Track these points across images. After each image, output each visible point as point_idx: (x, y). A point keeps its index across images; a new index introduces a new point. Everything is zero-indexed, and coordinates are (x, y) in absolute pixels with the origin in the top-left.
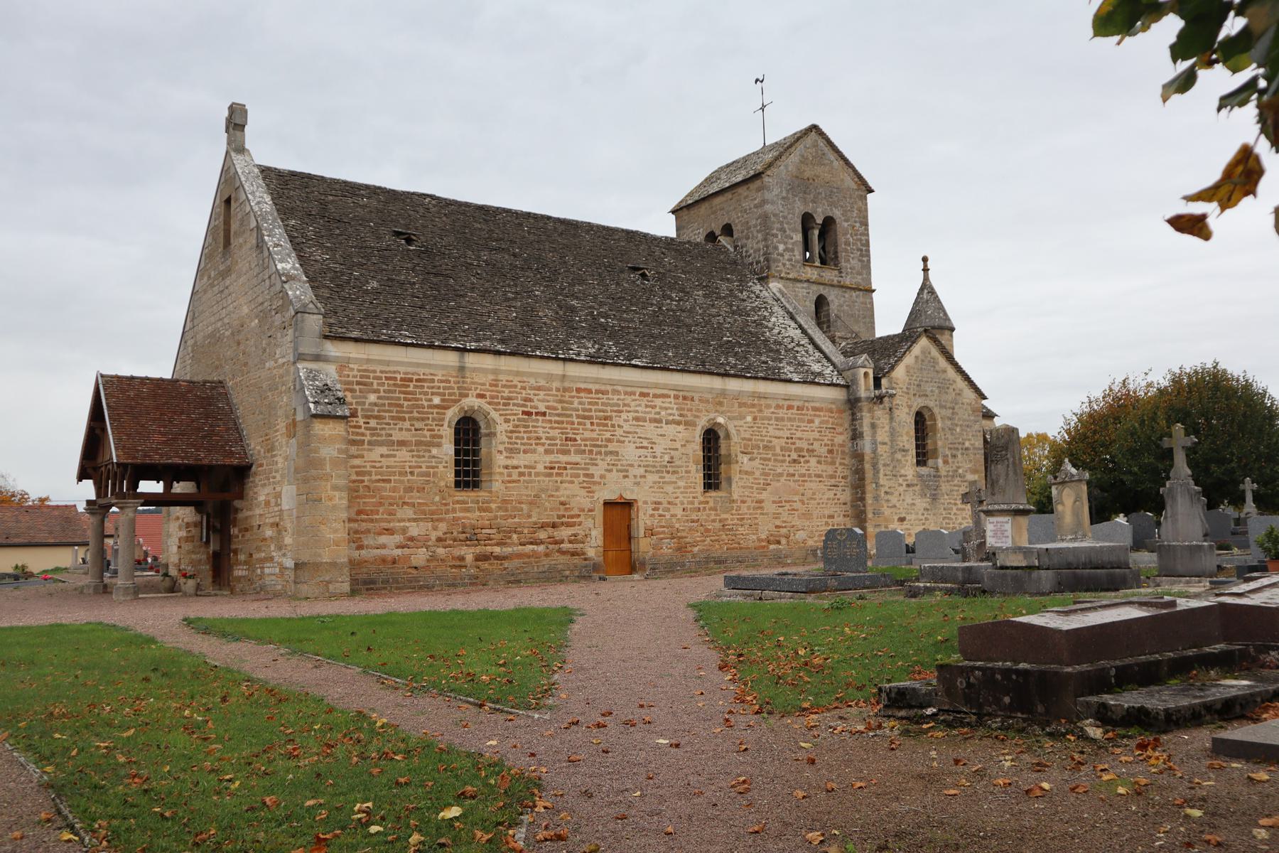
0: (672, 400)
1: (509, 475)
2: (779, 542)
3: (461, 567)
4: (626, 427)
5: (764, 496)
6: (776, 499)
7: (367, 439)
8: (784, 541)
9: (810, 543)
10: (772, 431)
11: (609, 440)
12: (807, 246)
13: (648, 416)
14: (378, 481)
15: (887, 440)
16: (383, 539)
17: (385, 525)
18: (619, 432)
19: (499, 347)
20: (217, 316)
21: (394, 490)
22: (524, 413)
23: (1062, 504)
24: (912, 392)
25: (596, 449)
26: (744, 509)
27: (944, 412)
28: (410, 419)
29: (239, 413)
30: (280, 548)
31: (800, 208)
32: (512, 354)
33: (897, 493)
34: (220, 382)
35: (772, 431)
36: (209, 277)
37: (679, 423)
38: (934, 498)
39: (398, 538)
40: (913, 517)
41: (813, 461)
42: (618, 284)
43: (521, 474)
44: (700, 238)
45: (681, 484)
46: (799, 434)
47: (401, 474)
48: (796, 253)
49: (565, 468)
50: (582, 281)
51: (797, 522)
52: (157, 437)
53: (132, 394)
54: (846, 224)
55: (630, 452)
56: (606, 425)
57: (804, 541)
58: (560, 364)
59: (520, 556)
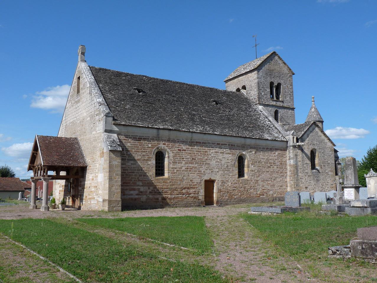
0: (228, 146)
1: (174, 171)
3: (157, 202)
4: (212, 155)
7: (127, 158)
8: (265, 195)
12: (272, 93)
13: (219, 151)
14: (131, 172)
15: (301, 160)
16: (132, 192)
17: (132, 187)
19: (170, 128)
20: (75, 116)
21: (136, 175)
22: (179, 150)
23: (370, 184)
24: (309, 143)
25: (201, 163)
26: (252, 183)
28: (141, 152)
29: (82, 149)
30: (97, 195)
31: (269, 80)
32: (175, 130)
34: (76, 138)
36: (72, 103)
38: (318, 181)
39: (137, 192)
41: (275, 167)
42: (208, 106)
43: (178, 171)
44: (234, 90)
46: (271, 158)
47: (138, 170)
48: (268, 95)
49: (192, 169)
50: (196, 105)
51: (269, 188)
52: (56, 157)
53: (47, 142)
55: (213, 163)
56: (206, 154)
58: (191, 133)
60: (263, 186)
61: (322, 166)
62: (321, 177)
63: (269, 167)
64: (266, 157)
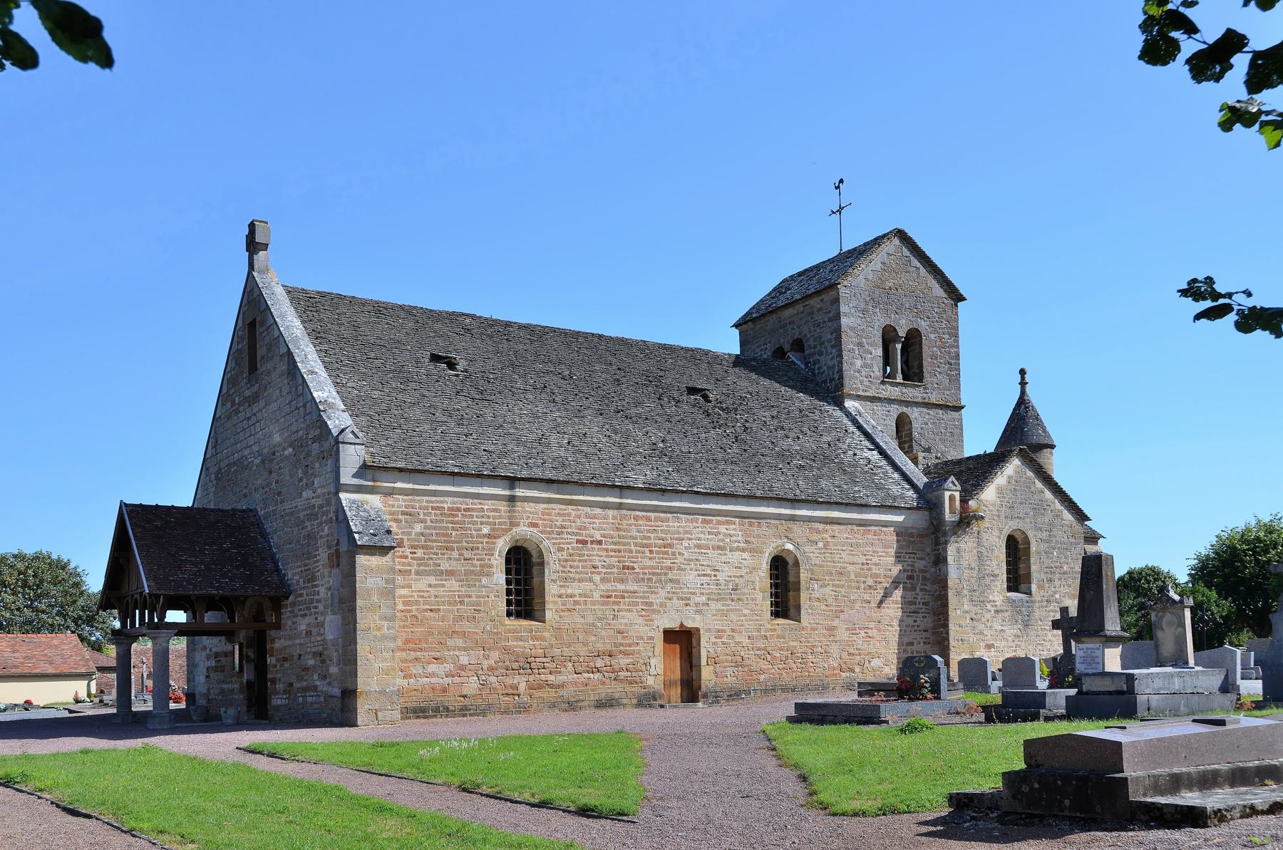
2: (853, 671)
5: (836, 623)
6: (851, 626)
8: (857, 669)
18: (680, 559)
27: (1039, 535)
31: (880, 321)
37: (743, 550)
46: (875, 560)
54: (932, 336)
55: (691, 578)
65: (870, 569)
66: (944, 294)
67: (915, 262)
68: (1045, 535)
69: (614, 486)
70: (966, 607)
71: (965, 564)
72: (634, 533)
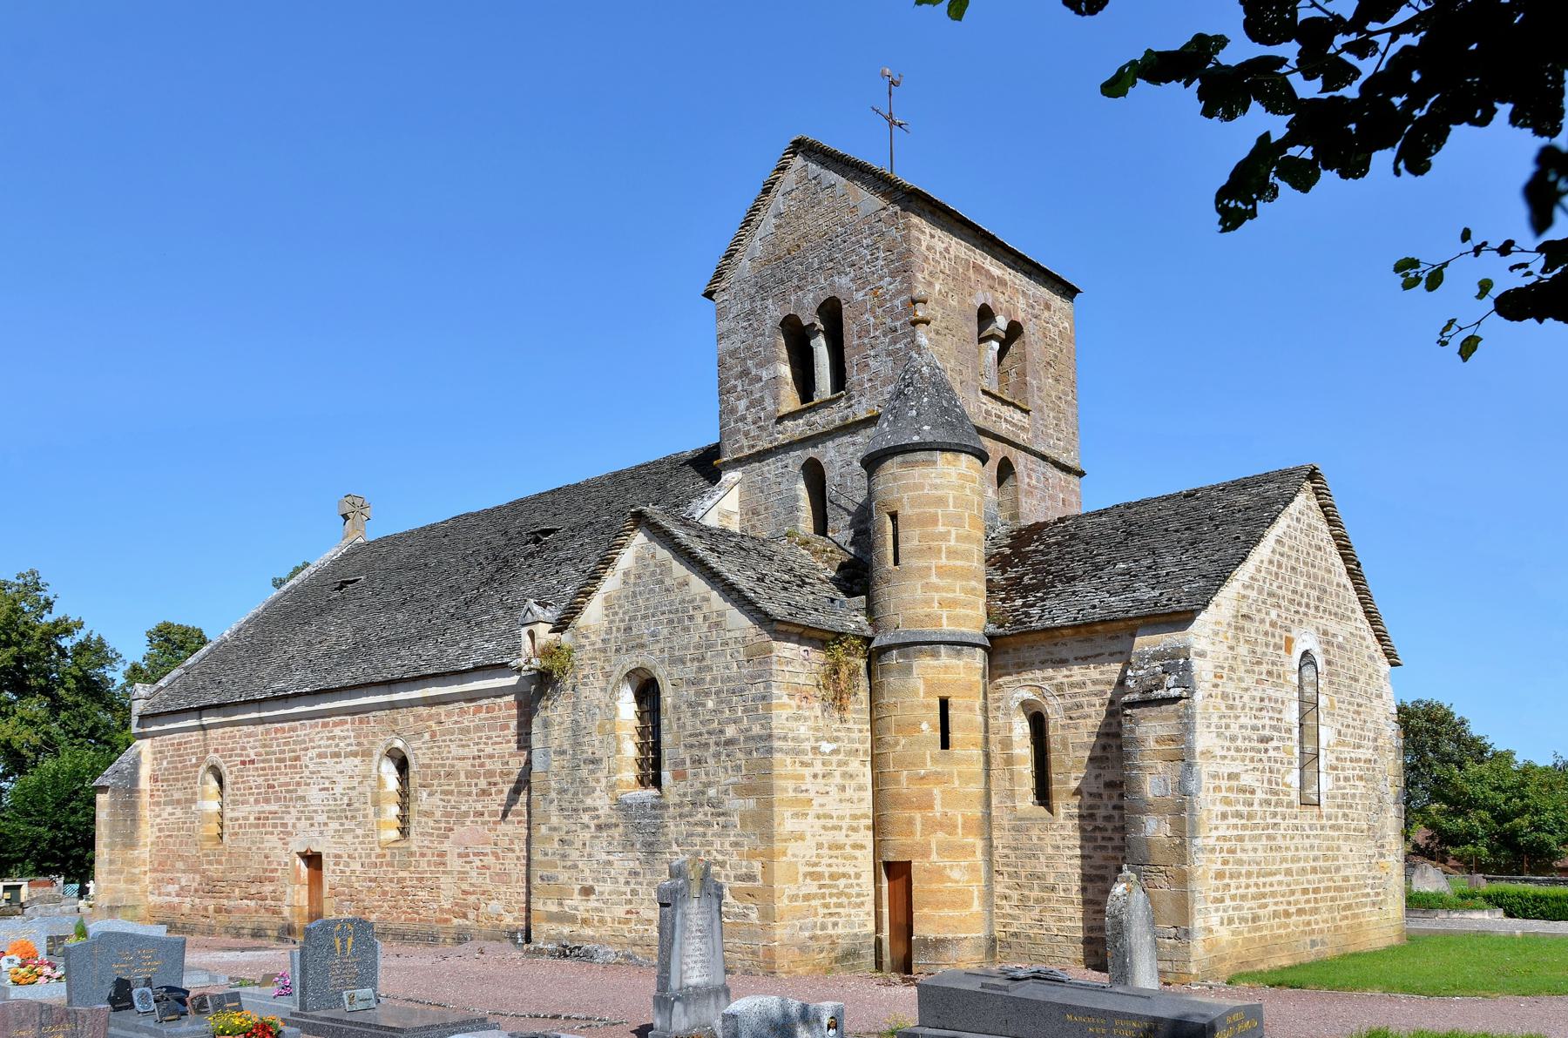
2: (465, 916)
5: (446, 846)
6: (462, 850)
8: (471, 915)
9: (508, 919)
10: (456, 750)
11: (298, 784)
18: (307, 773)
26: (424, 865)
27: (677, 671)
31: (775, 312)
33: (578, 844)
35: (456, 750)
37: (355, 754)
40: (607, 887)
45: (359, 832)
46: (489, 750)
54: (859, 296)
55: (314, 795)
57: (499, 917)
59: (239, 909)
60: (463, 876)
61: (683, 762)
62: (673, 829)
63: (484, 792)
64: (474, 751)
65: (482, 765)
66: (879, 202)
67: (832, 177)
68: (690, 670)
69: (255, 701)
70: (555, 820)
71: (555, 744)
72: (275, 748)
